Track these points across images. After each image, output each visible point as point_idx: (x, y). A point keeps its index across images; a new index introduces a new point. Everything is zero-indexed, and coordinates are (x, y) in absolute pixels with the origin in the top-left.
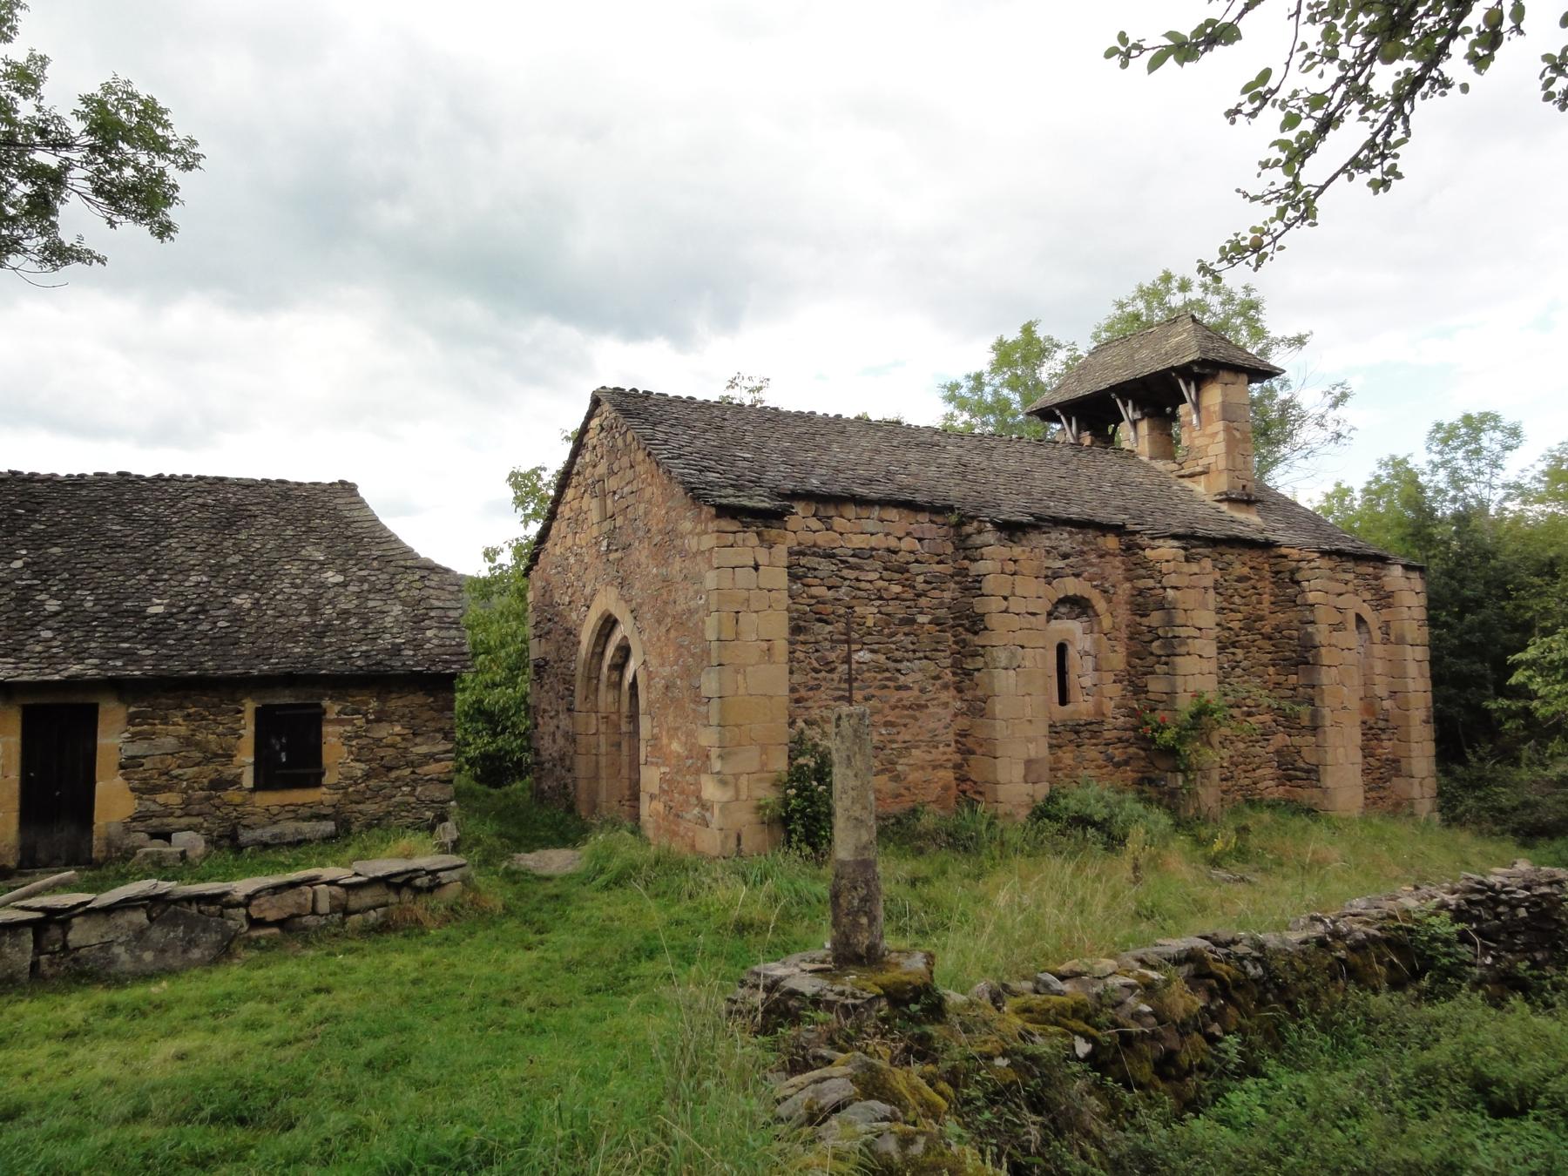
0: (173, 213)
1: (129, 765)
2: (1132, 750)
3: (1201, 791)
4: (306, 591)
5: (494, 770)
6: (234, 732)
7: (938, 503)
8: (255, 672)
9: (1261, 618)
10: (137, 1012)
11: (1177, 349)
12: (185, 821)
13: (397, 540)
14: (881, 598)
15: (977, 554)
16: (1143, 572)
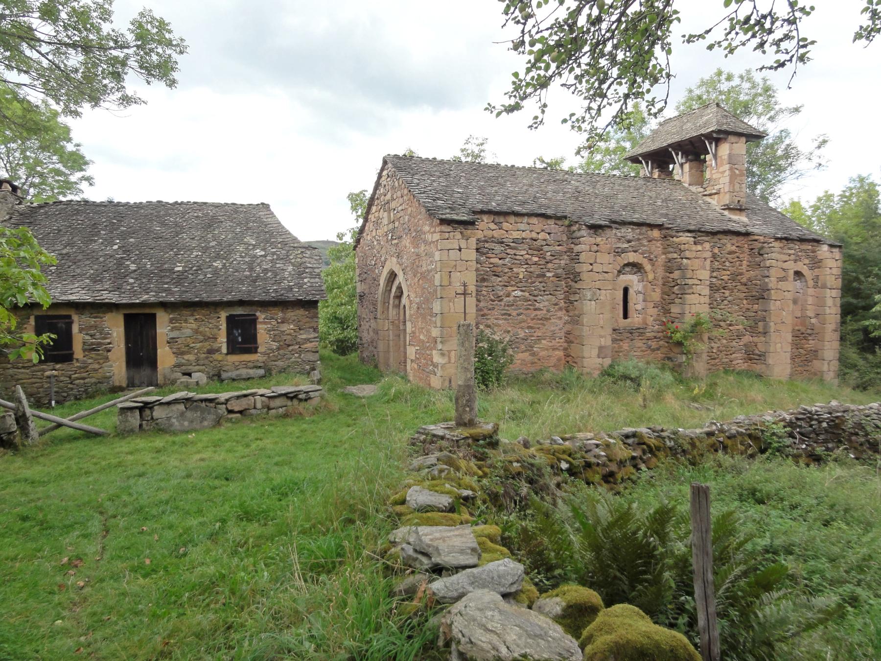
0: (175, 75)
1: (171, 342)
2: (661, 343)
3: (695, 364)
4: (247, 260)
5: (343, 347)
6: (217, 327)
7: (559, 215)
8: (225, 299)
9: (741, 274)
10: (184, 444)
11: (705, 124)
12: (197, 368)
13: (289, 233)
14: (527, 264)
15: (577, 241)
16: (672, 250)
